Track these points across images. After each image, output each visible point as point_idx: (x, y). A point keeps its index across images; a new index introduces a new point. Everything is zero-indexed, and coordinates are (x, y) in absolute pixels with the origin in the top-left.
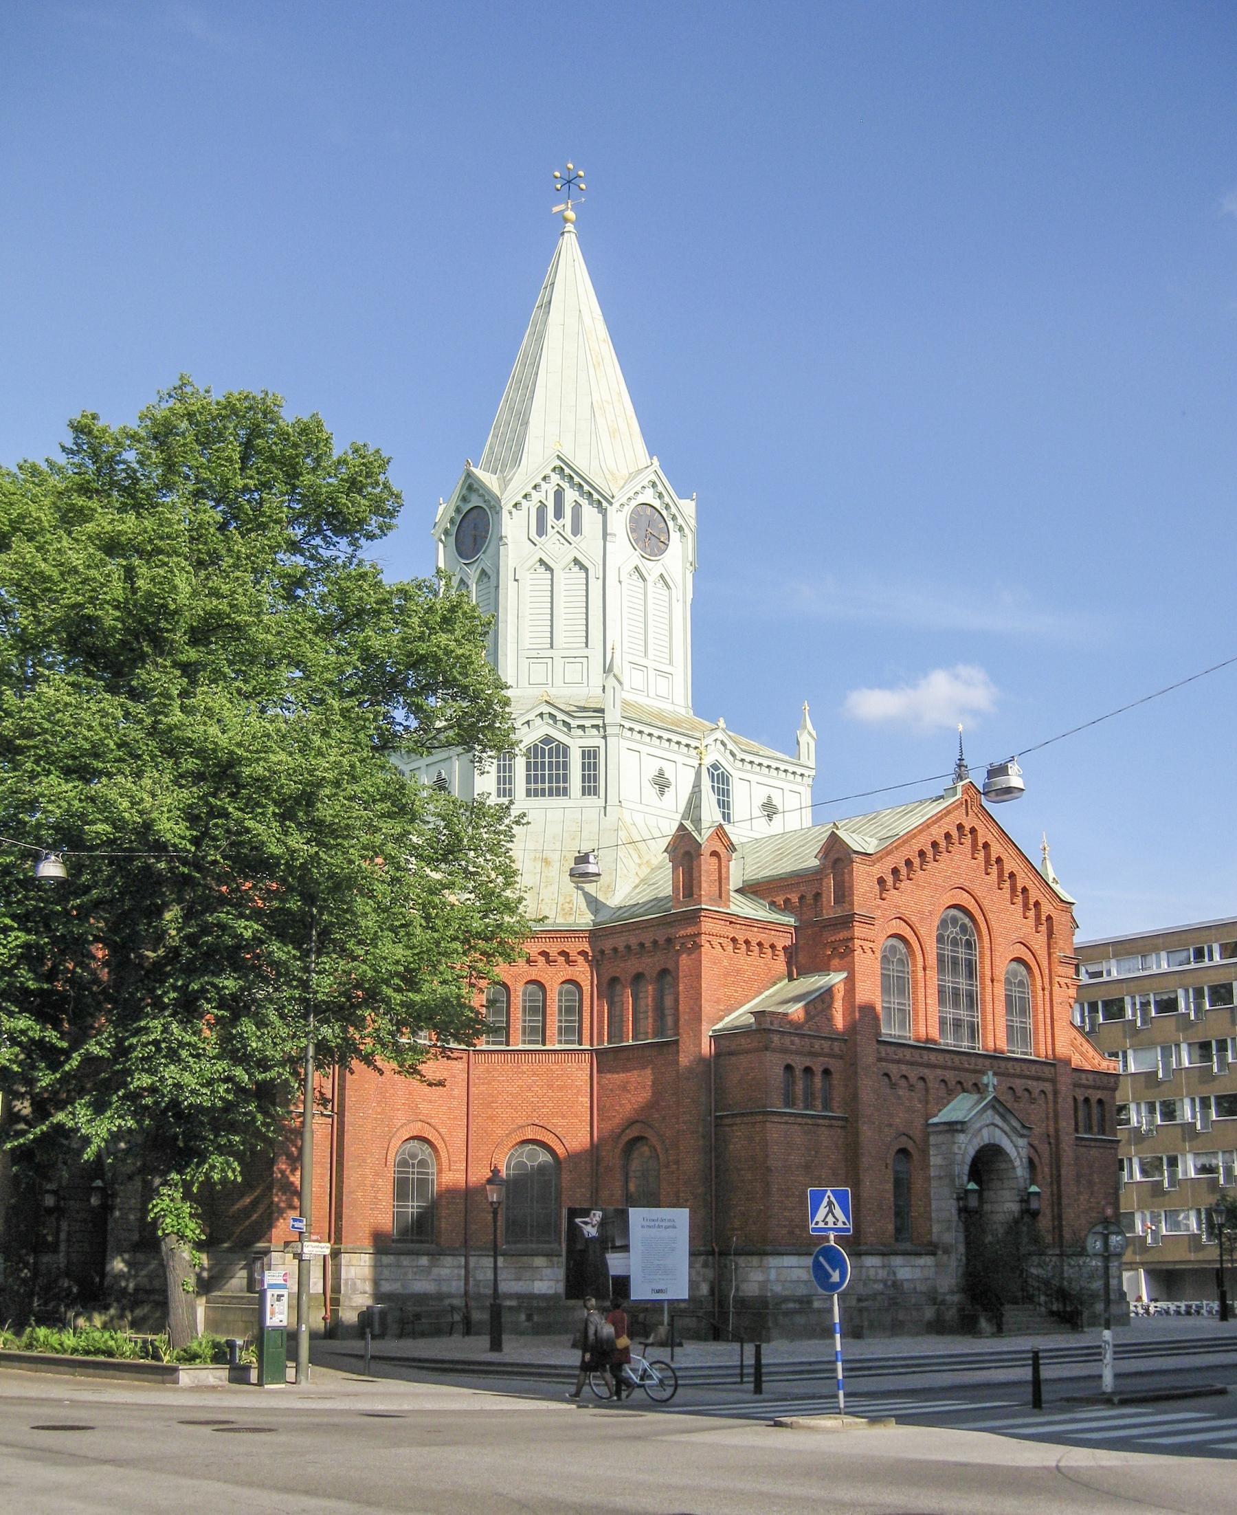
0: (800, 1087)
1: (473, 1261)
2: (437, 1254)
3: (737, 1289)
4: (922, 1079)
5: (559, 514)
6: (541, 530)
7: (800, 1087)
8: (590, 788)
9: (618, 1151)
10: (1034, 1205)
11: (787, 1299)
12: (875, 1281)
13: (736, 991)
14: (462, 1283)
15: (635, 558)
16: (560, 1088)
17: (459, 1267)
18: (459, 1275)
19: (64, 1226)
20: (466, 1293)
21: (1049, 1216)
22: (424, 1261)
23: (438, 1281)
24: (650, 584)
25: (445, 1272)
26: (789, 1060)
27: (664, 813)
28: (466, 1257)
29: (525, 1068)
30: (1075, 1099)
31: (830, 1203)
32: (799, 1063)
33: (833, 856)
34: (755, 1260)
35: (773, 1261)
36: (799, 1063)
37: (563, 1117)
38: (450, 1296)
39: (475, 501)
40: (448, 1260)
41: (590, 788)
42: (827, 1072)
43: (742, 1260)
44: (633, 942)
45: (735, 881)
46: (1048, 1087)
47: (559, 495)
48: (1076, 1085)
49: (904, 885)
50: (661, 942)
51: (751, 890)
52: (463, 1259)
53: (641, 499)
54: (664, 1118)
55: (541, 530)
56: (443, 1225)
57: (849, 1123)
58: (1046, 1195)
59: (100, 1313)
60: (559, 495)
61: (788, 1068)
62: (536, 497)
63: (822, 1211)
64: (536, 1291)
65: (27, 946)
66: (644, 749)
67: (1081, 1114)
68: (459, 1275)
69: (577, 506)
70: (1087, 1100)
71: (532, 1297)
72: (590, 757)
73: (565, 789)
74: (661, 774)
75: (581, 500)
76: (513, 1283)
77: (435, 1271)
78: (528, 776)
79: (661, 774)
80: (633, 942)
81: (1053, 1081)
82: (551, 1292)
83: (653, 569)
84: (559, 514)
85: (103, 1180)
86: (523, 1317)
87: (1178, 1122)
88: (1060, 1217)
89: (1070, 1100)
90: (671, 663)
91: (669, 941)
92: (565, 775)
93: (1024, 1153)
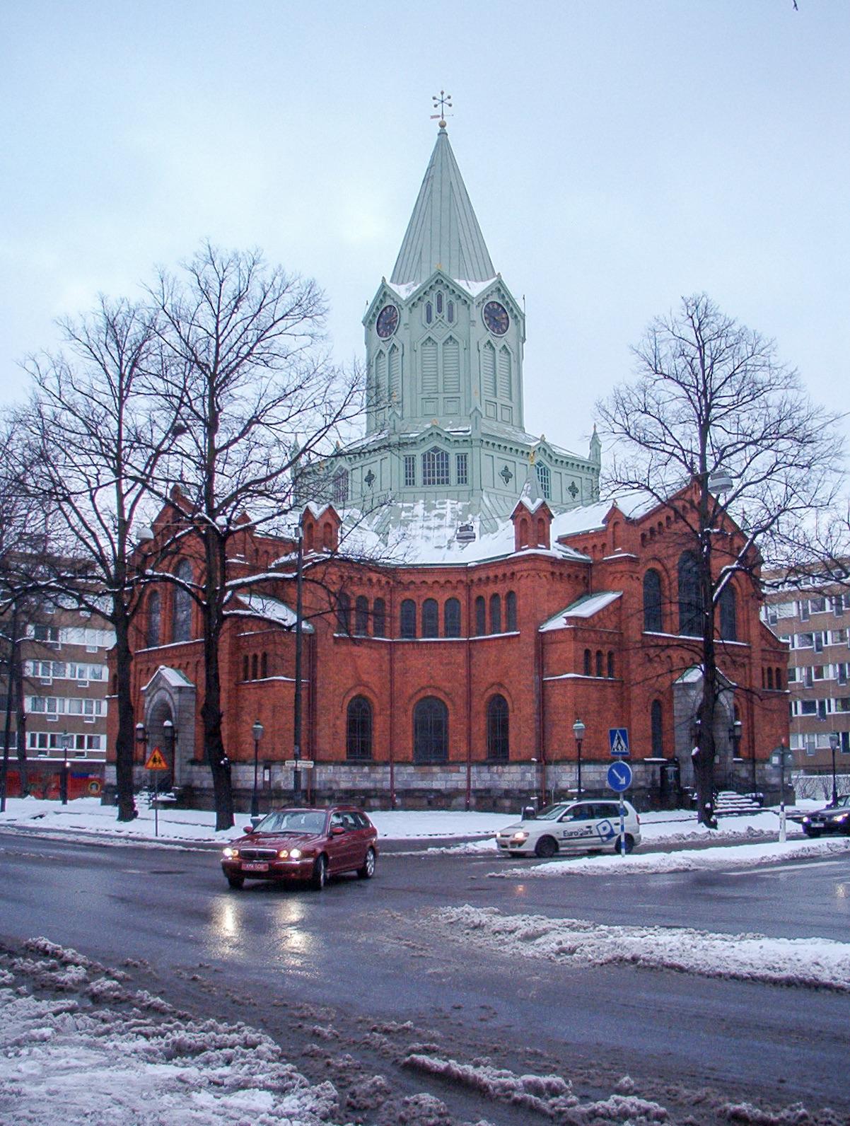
0: (594, 662)
1: (395, 769)
2: (374, 764)
4: (669, 657)
5: (440, 310)
6: (429, 320)
7: (594, 662)
8: (462, 480)
9: (483, 702)
10: (738, 732)
12: (640, 780)
15: (488, 336)
19: (148, 749)
21: (746, 739)
22: (366, 769)
23: (375, 781)
24: (497, 352)
25: (378, 776)
26: (588, 646)
27: (508, 494)
30: (763, 669)
31: (619, 738)
32: (594, 649)
36: (594, 649)
39: (389, 302)
40: (380, 769)
41: (462, 480)
42: (599, 653)
43: (559, 769)
44: (491, 575)
45: (553, 537)
46: (746, 660)
47: (440, 297)
48: (764, 659)
49: (657, 538)
50: (508, 574)
51: (561, 540)
55: (429, 320)
57: (623, 686)
58: (744, 727)
59: (145, 541)
60: (440, 297)
61: (587, 652)
62: (427, 299)
63: (616, 743)
65: (464, 507)
66: (495, 455)
67: (766, 676)
69: (451, 306)
70: (770, 670)
72: (462, 459)
73: (447, 480)
74: (506, 469)
75: (454, 300)
77: (373, 775)
78: (425, 473)
79: (506, 469)
80: (483, 576)
81: (749, 657)
83: (499, 343)
84: (440, 310)
85: (170, 719)
87: (825, 679)
88: (753, 741)
89: (760, 669)
90: (511, 399)
91: (513, 574)
92: (447, 471)
93: (731, 701)
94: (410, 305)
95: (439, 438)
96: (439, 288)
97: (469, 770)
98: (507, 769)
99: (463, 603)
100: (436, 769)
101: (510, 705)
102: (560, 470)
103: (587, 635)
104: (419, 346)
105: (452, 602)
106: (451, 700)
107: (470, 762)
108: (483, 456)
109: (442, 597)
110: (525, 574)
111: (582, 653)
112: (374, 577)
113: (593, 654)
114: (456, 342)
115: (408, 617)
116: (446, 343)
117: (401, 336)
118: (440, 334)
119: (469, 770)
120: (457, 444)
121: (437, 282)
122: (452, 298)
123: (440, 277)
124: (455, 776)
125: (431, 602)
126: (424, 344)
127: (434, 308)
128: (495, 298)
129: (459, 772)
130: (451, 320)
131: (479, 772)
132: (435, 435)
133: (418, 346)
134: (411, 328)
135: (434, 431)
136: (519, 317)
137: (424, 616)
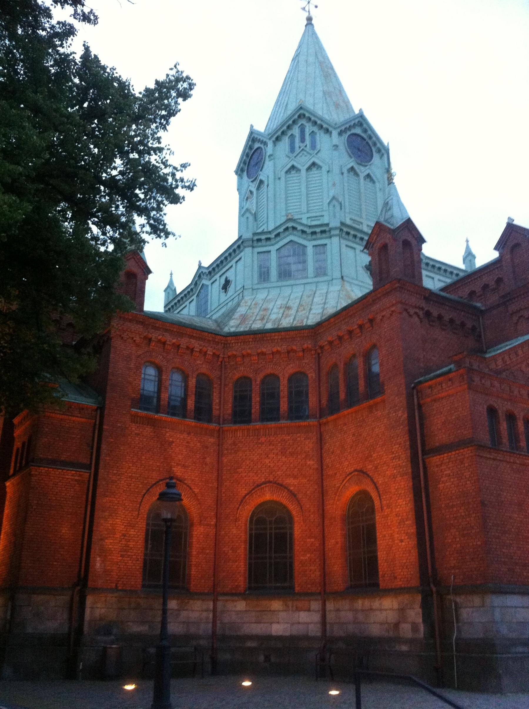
1: (220, 604)
3: (459, 631)
5: (303, 140)
11: (514, 642)
13: (434, 356)
14: (210, 625)
16: (292, 454)
17: (207, 610)
18: (207, 618)
20: (214, 632)
25: (194, 615)
26: (493, 401)
28: (215, 601)
29: (263, 439)
33: (510, 244)
34: (477, 600)
35: (497, 600)
36: (503, 407)
37: (295, 477)
38: (197, 637)
39: (257, 145)
52: (211, 604)
53: (353, 131)
54: (376, 468)
55: (292, 149)
56: (193, 573)
61: (492, 411)
64: (274, 634)
68: (207, 618)
71: (269, 638)
76: (254, 626)
77: (184, 614)
82: (287, 634)
83: (363, 171)
84: (303, 140)
86: (262, 658)
94: (274, 139)
95: (295, 232)
96: (303, 121)
97: (324, 605)
98: (376, 604)
99: (312, 375)
100: (276, 605)
101: (377, 503)
102: (432, 275)
103: (488, 383)
104: (283, 173)
105: (297, 379)
106: (299, 503)
107: (325, 593)
108: (343, 246)
109: (285, 371)
110: (387, 313)
111: (483, 410)
112: (196, 345)
113: (501, 414)
114: (319, 167)
115: (242, 399)
116: (309, 169)
117: (268, 171)
118: (303, 162)
119: (324, 605)
120: (314, 237)
121: (299, 117)
122: (315, 129)
123: (301, 111)
124: (303, 616)
125: (271, 380)
126: (288, 172)
127: (297, 140)
128: (358, 131)
129: (309, 610)
130: (313, 146)
131: (338, 610)
132: (290, 230)
133: (345, 170)
134: (278, 157)
135: (290, 224)
136: (384, 151)
137: (262, 395)
